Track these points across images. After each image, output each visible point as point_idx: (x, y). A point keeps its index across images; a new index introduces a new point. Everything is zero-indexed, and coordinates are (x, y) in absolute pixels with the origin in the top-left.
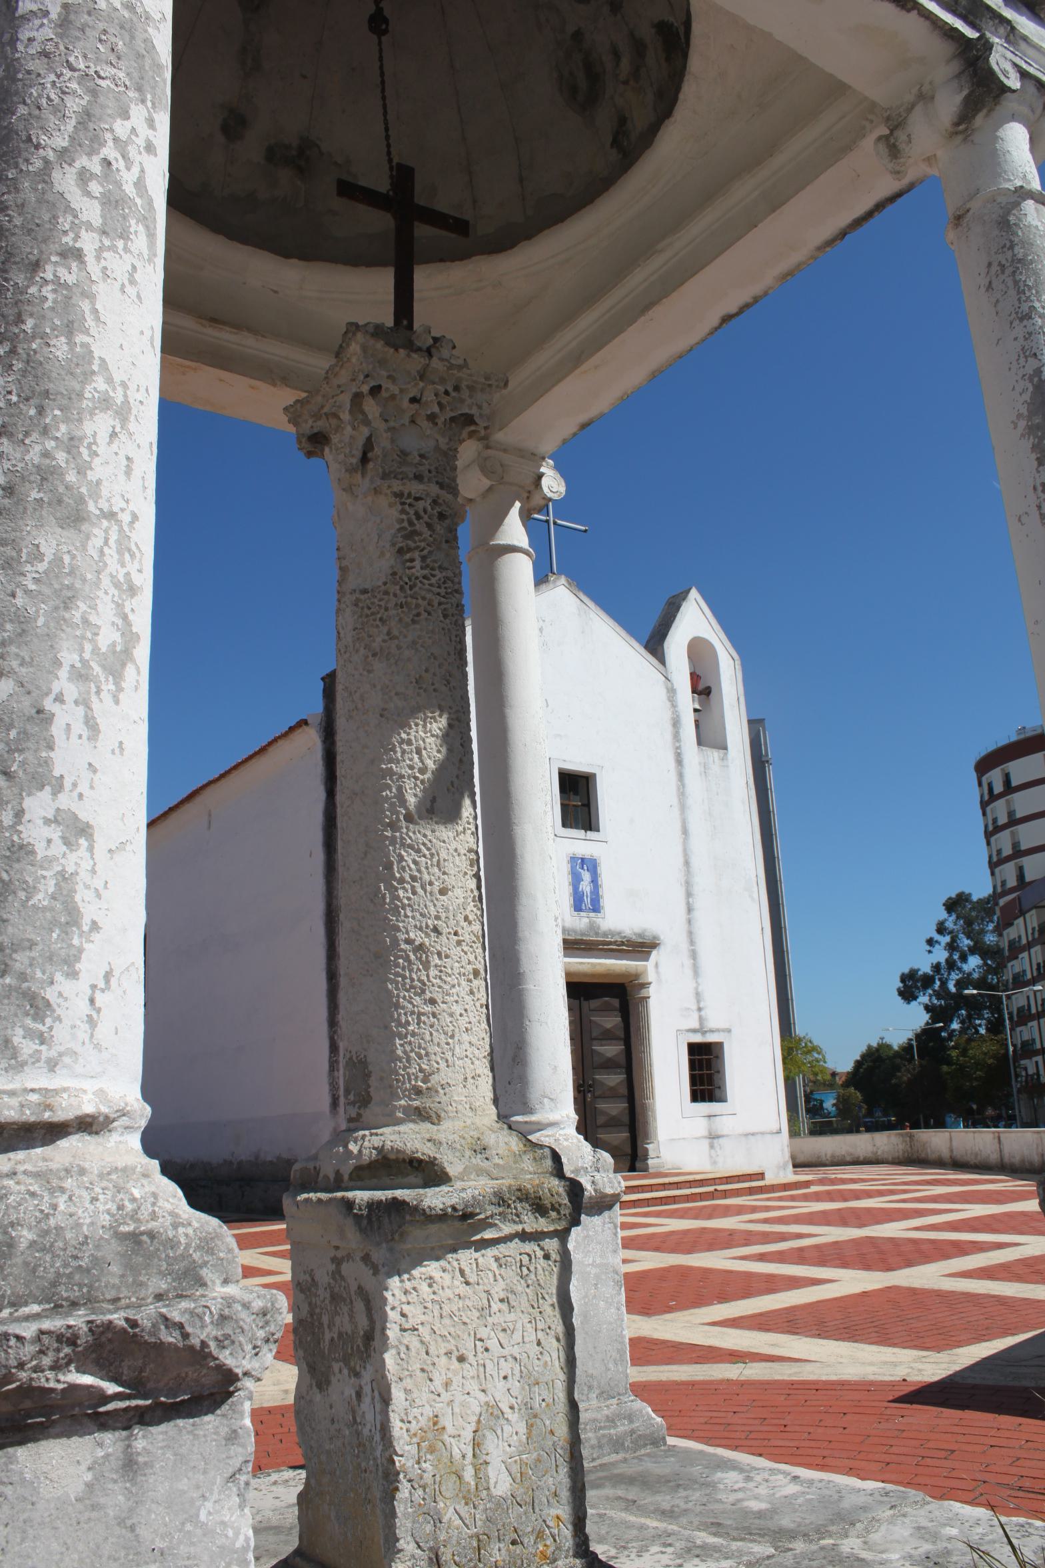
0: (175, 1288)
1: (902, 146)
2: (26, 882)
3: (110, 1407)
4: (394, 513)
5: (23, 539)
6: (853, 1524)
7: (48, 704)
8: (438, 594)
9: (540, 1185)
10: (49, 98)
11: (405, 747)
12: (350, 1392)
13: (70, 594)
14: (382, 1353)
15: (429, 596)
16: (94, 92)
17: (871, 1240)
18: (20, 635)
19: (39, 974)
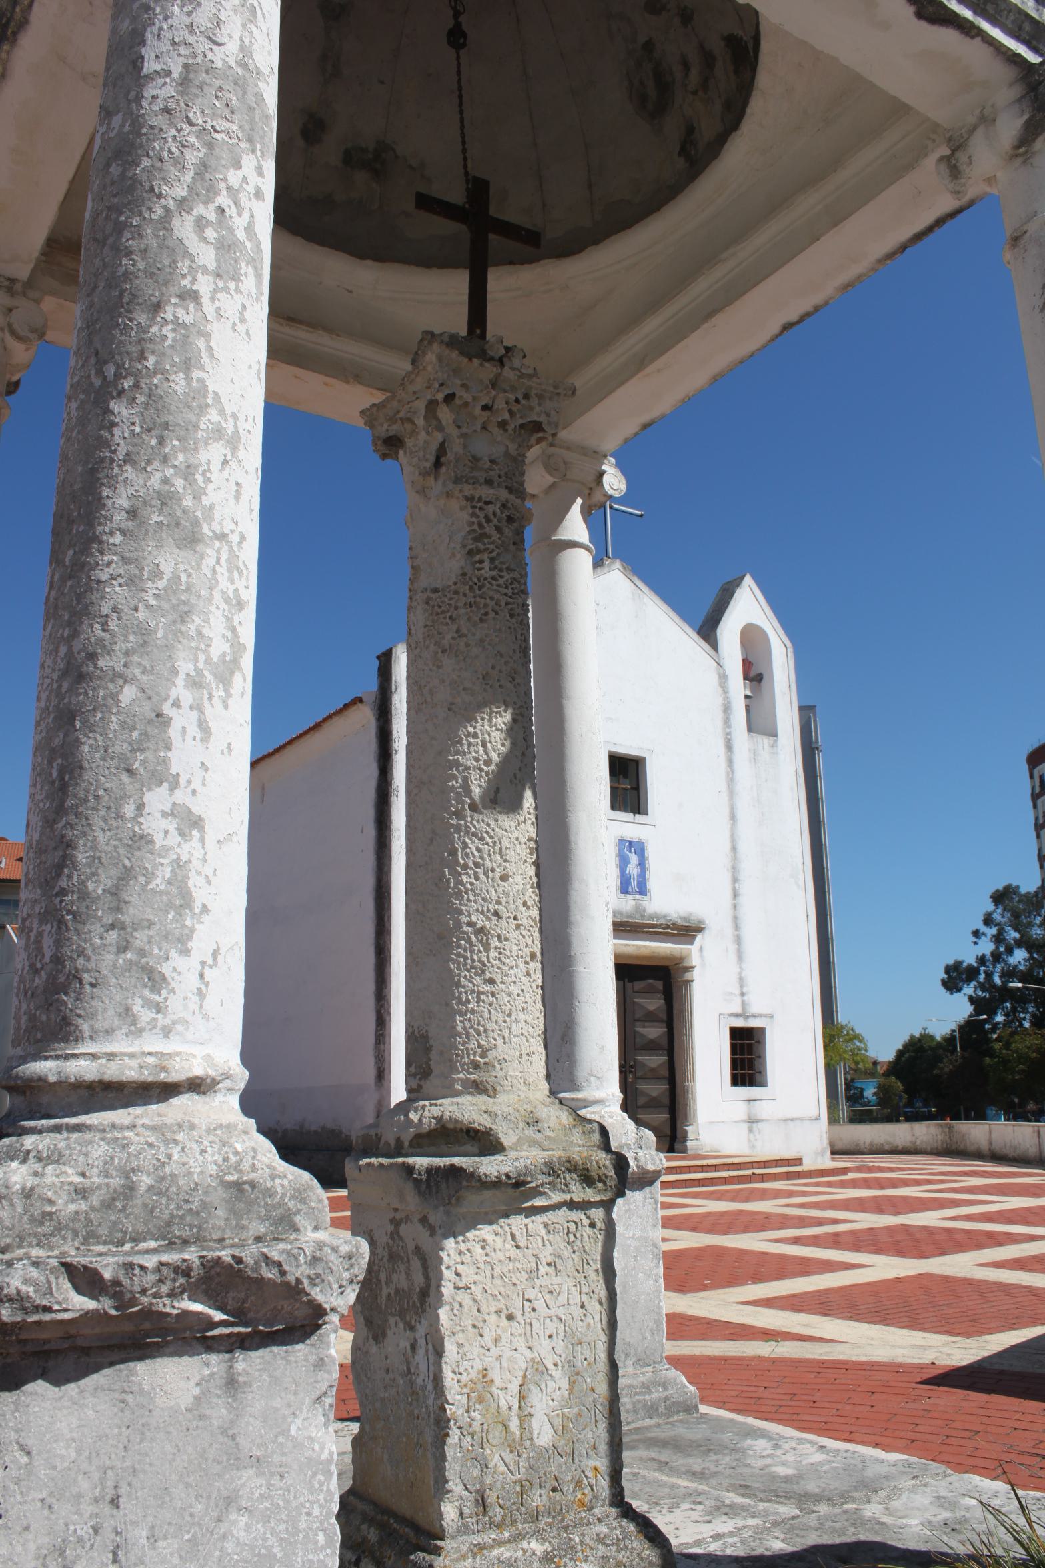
0: (272, 1232)
1: (963, 167)
2: (145, 868)
3: (216, 1332)
4: (465, 516)
5: (145, 558)
6: (876, 1491)
7: (166, 709)
8: (505, 594)
9: (589, 1158)
10: (170, 152)
11: (471, 740)
12: (405, 1344)
13: (186, 609)
14: (436, 1309)
15: (496, 596)
16: (210, 145)
17: (906, 1228)
18: (142, 646)
19: (156, 951)
